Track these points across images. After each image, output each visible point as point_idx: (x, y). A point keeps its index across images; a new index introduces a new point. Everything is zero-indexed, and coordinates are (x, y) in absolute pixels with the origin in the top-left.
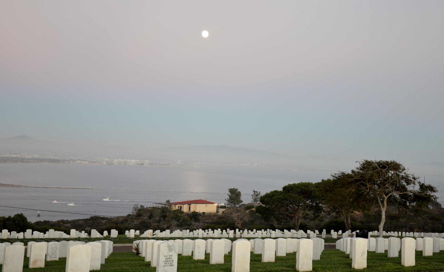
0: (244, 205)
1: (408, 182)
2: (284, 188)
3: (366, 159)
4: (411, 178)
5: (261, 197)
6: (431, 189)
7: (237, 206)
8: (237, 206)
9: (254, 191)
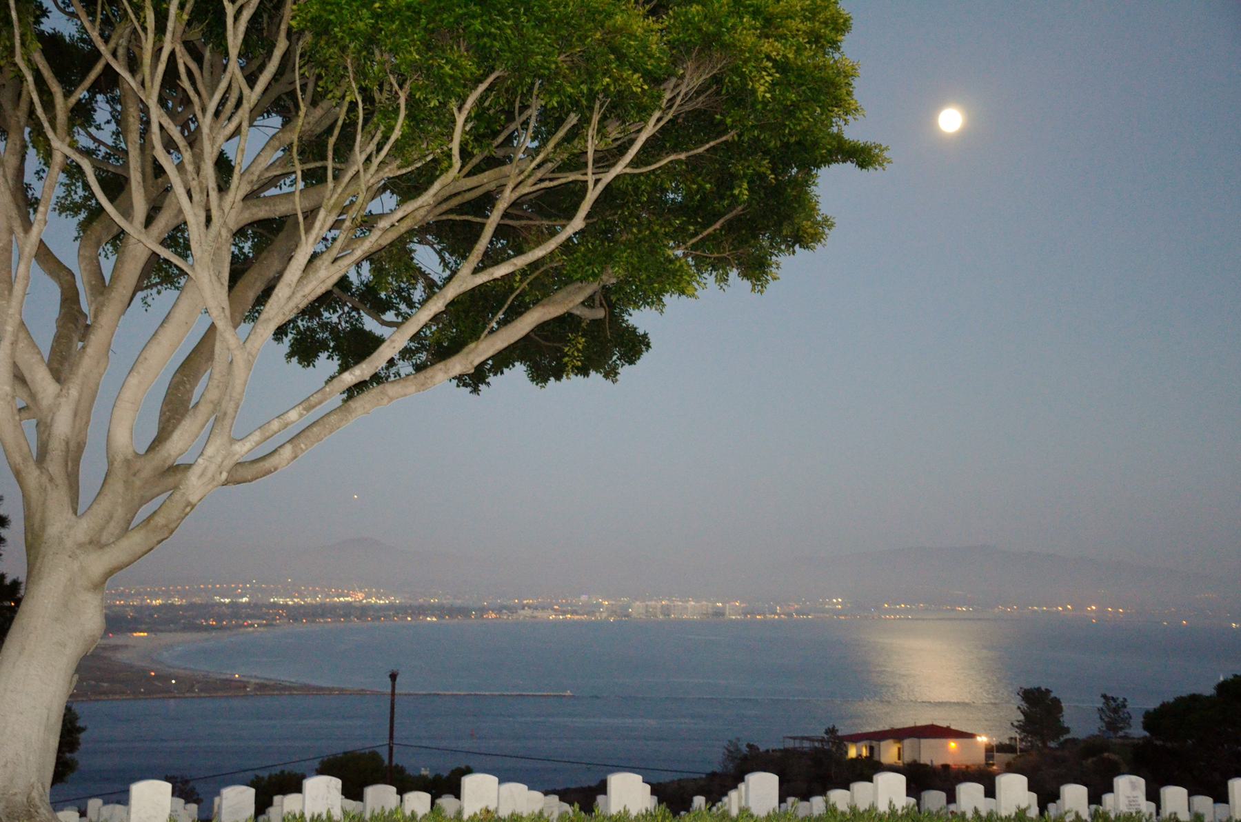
2: (1222, 687)
7: (1052, 744)
8: (1052, 744)
9: (1104, 696)
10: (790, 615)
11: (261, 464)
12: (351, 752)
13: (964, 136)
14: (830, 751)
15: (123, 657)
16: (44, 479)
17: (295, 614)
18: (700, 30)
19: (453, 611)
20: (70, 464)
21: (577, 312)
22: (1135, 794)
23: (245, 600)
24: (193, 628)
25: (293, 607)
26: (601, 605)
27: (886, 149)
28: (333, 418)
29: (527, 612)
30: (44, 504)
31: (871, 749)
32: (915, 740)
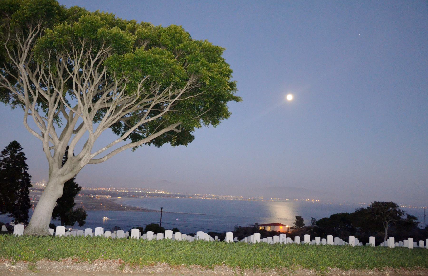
0: (305, 227)
1: (401, 214)
2: (332, 216)
3: (375, 200)
4: (401, 212)
5: (317, 221)
6: (414, 218)
7: (301, 227)
8: (301, 227)
9: (312, 218)
10: (252, 200)
11: (103, 159)
12: (153, 224)
14: (256, 228)
15: (116, 202)
16: (53, 160)
17: (150, 195)
18: (193, 69)
19: (182, 196)
20: (60, 158)
21: (175, 130)
22: (284, 238)
23: (140, 192)
24: (129, 197)
25: (150, 194)
26: (213, 196)
27: (242, 98)
28: (117, 150)
29: (197, 197)
30: (53, 166)
31: (265, 228)
32: (273, 226)
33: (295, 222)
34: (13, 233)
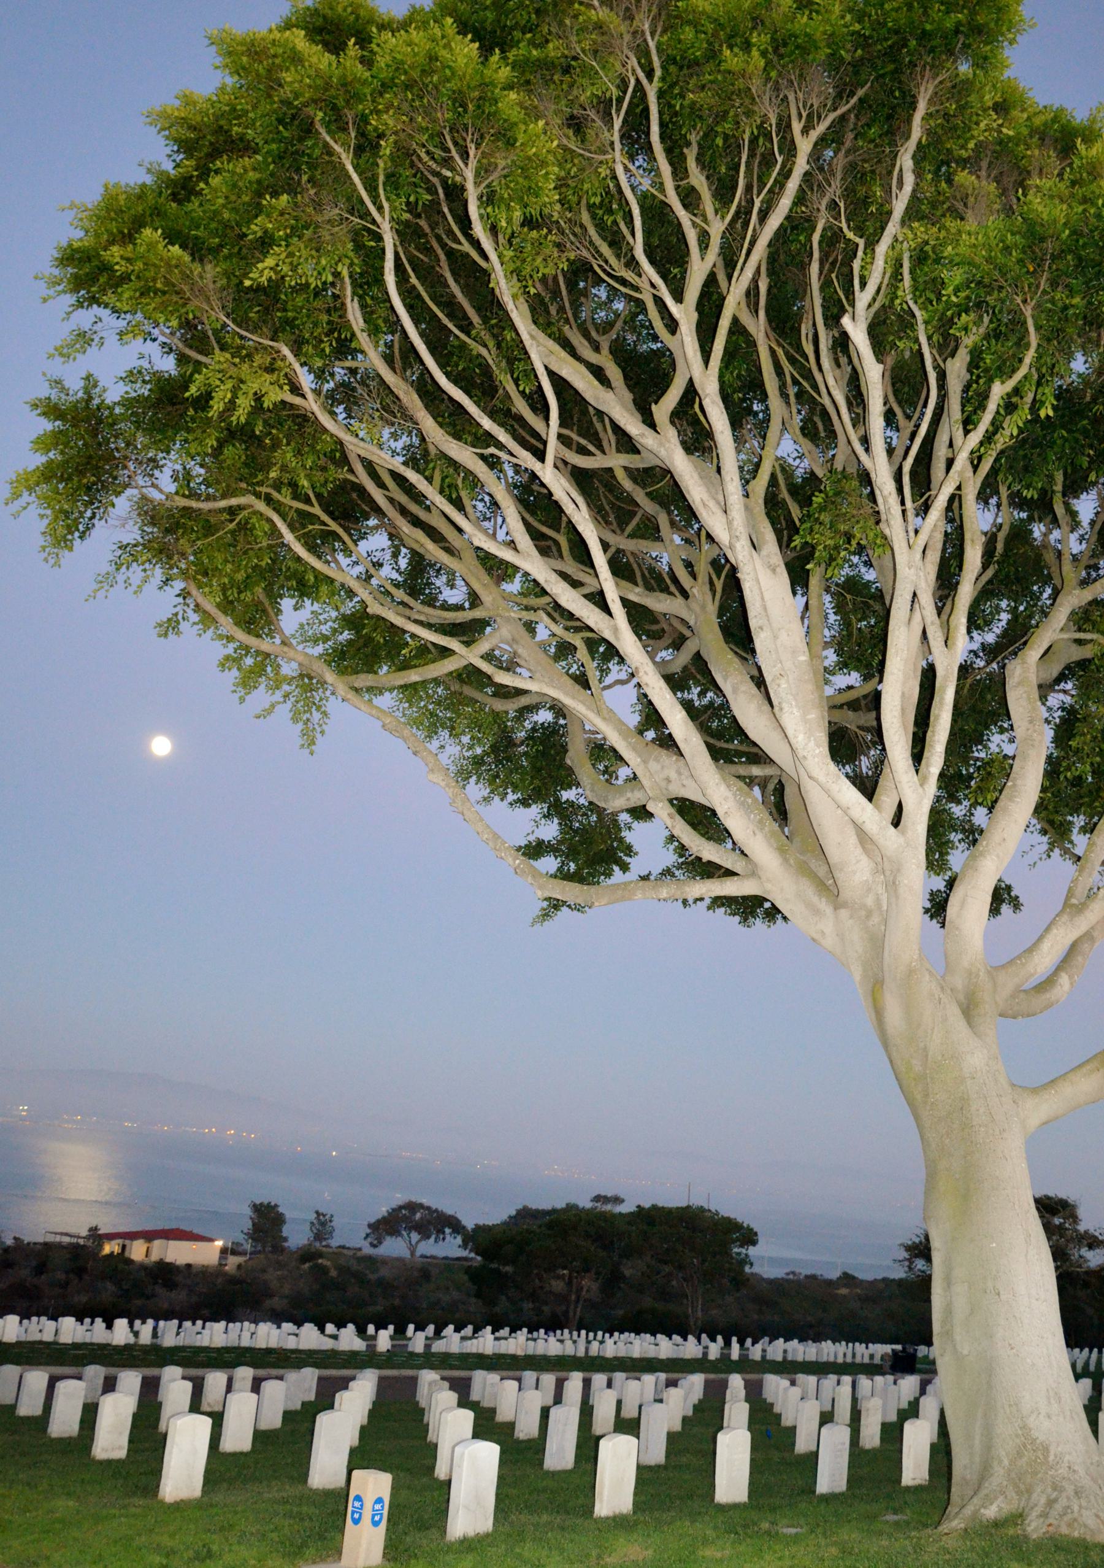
9: (317, 1212)
13: (166, 760)
33: (250, 1225)
34: (143, 1378)
